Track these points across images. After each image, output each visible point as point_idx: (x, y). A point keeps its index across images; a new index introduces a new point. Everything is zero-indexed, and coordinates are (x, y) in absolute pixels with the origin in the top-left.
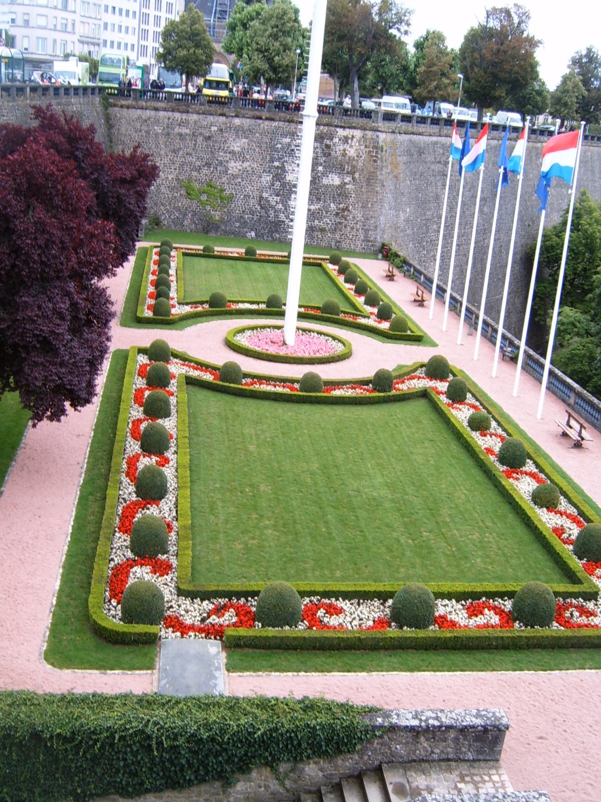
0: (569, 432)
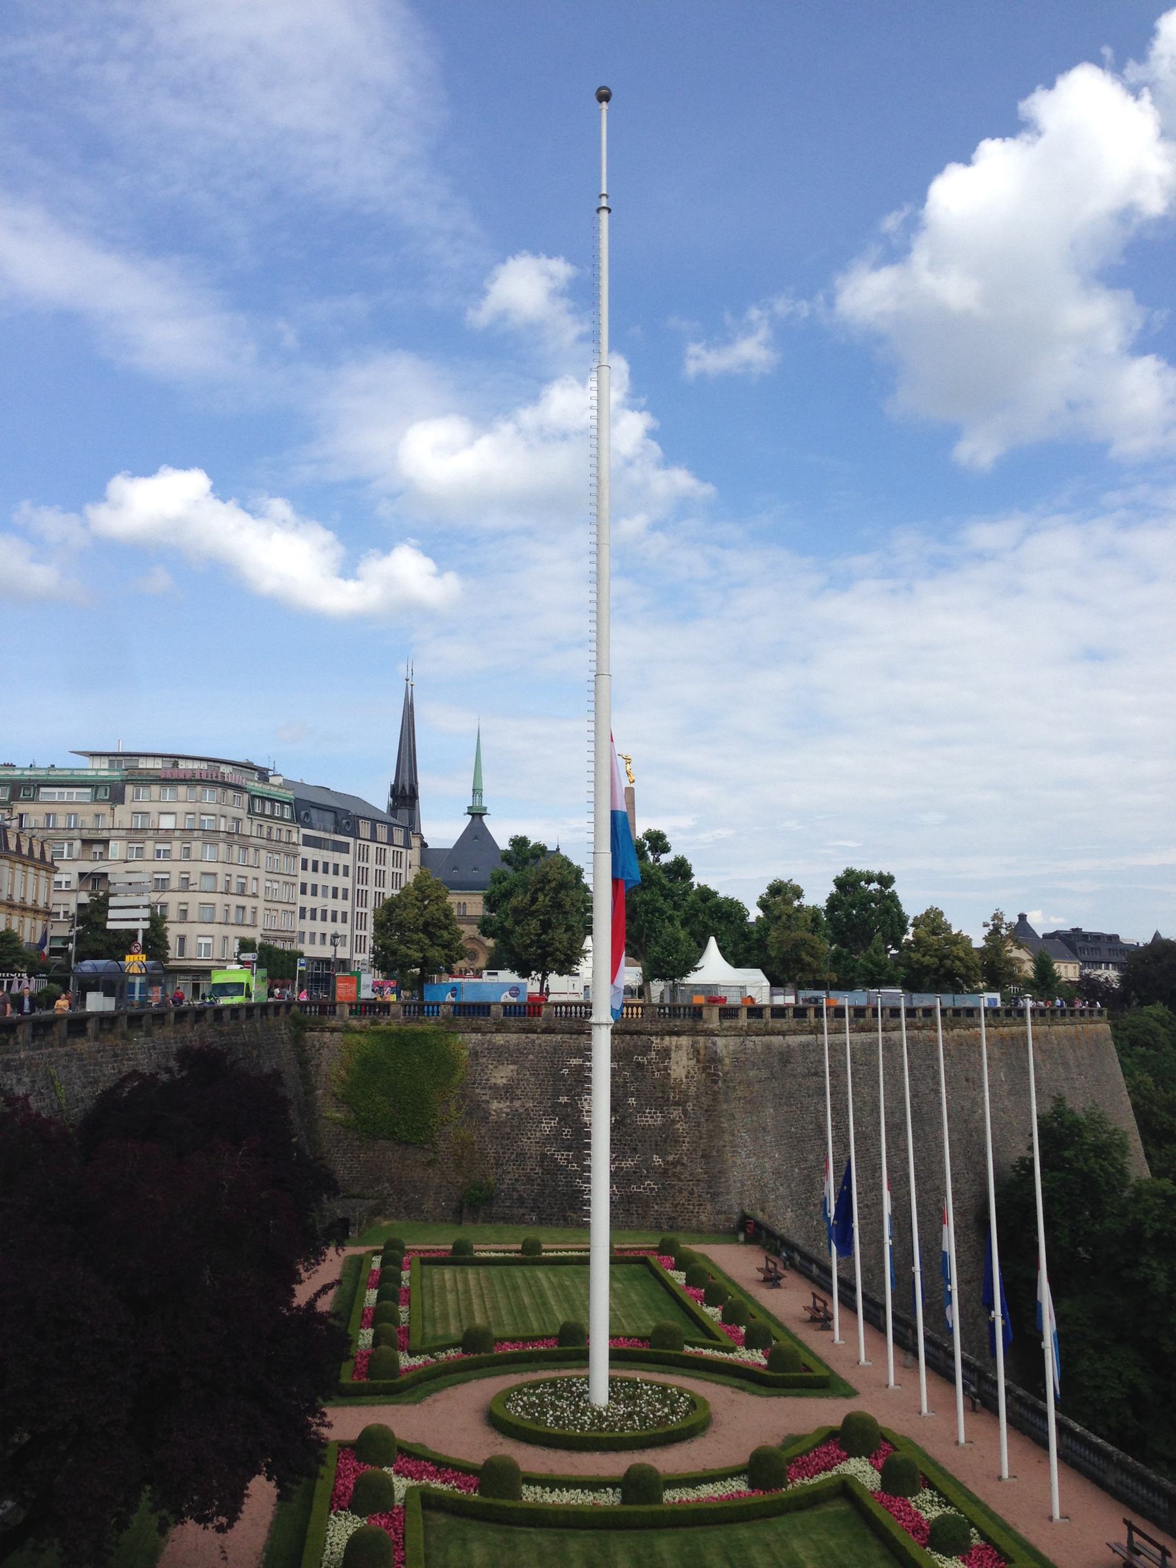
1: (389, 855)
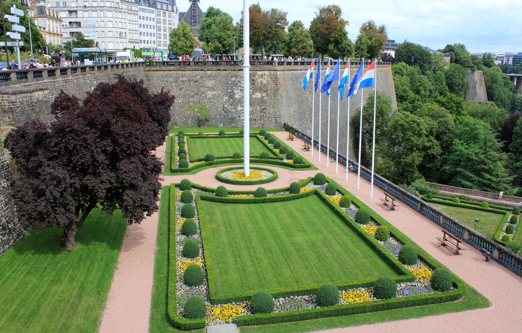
0: (387, 203)
1: (167, 14)
